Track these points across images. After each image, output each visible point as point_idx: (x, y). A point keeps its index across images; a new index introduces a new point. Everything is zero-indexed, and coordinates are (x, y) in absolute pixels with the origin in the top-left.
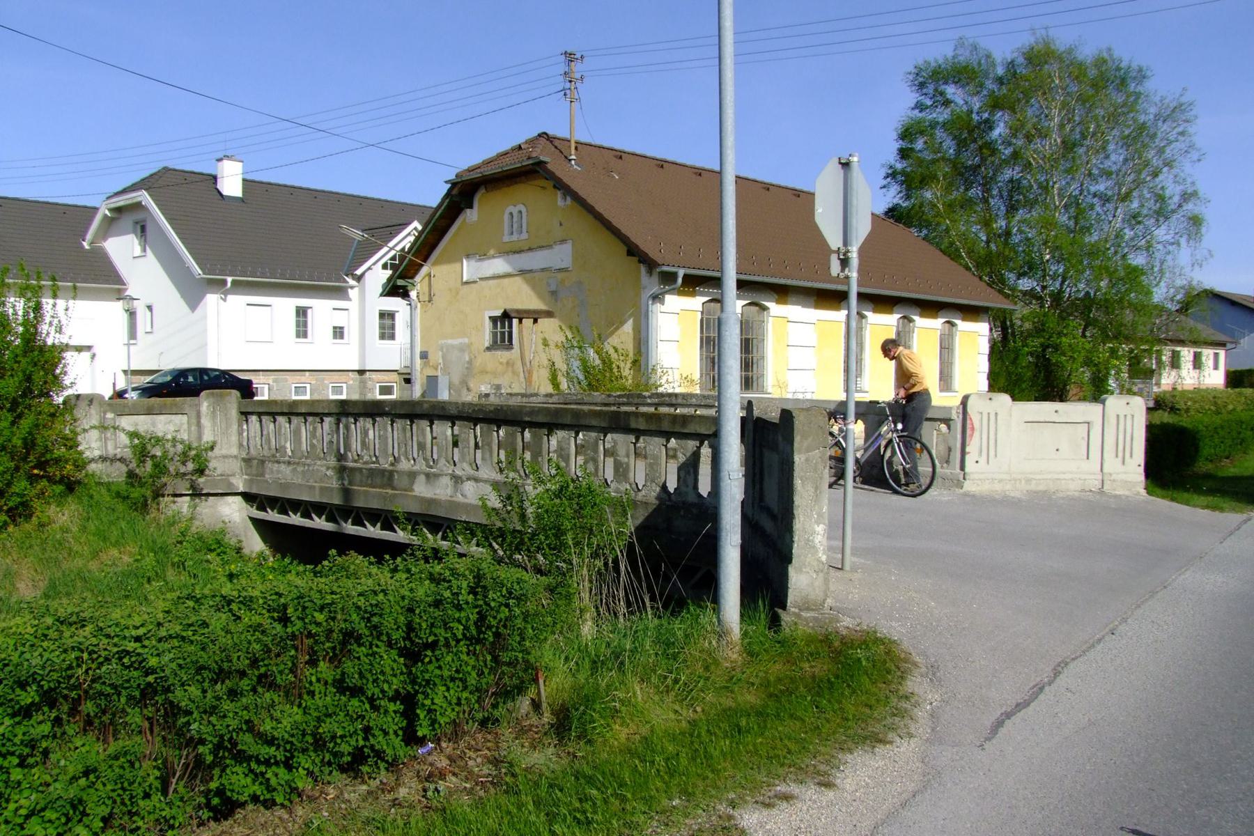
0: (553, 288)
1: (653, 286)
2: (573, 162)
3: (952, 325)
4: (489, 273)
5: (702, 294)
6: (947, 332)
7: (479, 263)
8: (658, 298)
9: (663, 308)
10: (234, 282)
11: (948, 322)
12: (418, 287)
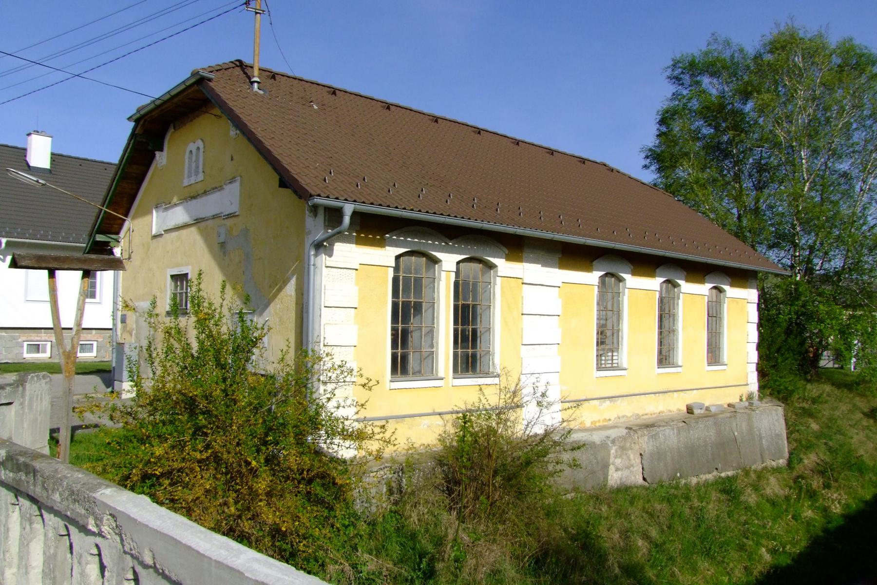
0: (222, 239)
1: (318, 230)
2: (256, 85)
3: (720, 290)
4: (171, 224)
5: (396, 244)
6: (714, 299)
7: (165, 213)
8: (322, 247)
9: (329, 261)
10: (8, 243)
11: (715, 288)
12: (122, 243)
